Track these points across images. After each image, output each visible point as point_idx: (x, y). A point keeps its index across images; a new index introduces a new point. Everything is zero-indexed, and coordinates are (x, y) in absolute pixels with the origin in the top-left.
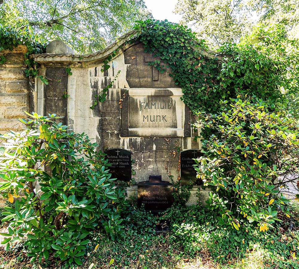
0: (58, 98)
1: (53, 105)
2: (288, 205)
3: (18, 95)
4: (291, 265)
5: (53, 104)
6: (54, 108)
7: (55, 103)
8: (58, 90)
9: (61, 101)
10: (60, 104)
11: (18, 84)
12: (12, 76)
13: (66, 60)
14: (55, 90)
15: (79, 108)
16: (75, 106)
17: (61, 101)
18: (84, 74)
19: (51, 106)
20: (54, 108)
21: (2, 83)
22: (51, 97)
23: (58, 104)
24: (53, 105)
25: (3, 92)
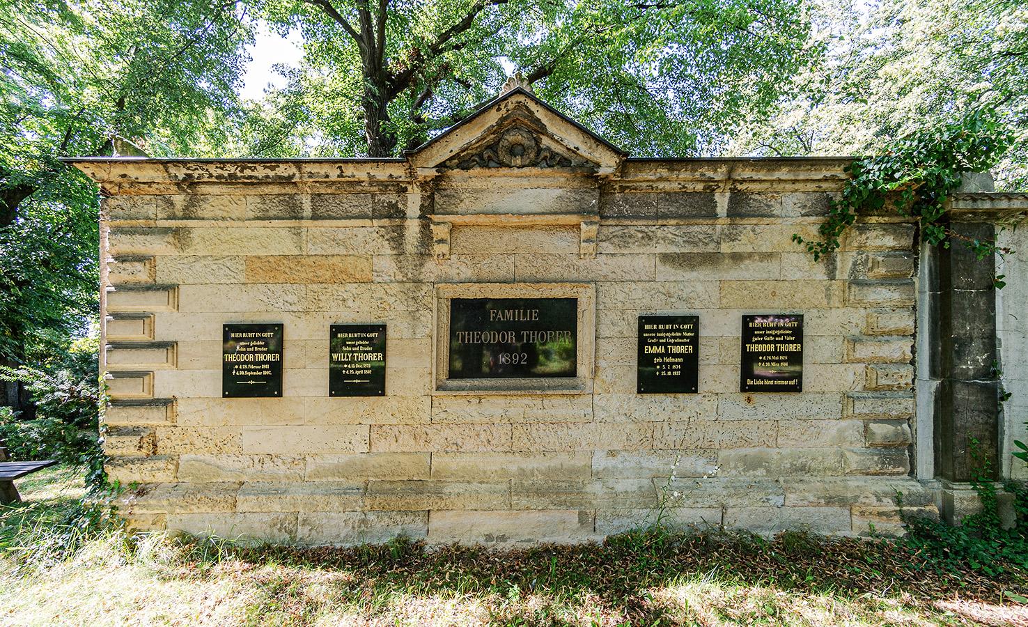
0: (978, 289)
1: (967, 306)
2: (113, 533)
3: (903, 284)
4: (543, 609)
5: (966, 303)
6: (968, 312)
7: (971, 301)
8: (976, 273)
9: (984, 298)
10: (982, 303)
11: (905, 261)
12: (890, 241)
13: (1021, 207)
14: (970, 275)
15: (1011, 312)
16: (1004, 307)
17: (984, 298)
18: (1022, 239)
19: (964, 309)
20: (968, 312)
21: (860, 257)
22: (963, 288)
23: (978, 305)
24: (967, 306)
25: (861, 278)
